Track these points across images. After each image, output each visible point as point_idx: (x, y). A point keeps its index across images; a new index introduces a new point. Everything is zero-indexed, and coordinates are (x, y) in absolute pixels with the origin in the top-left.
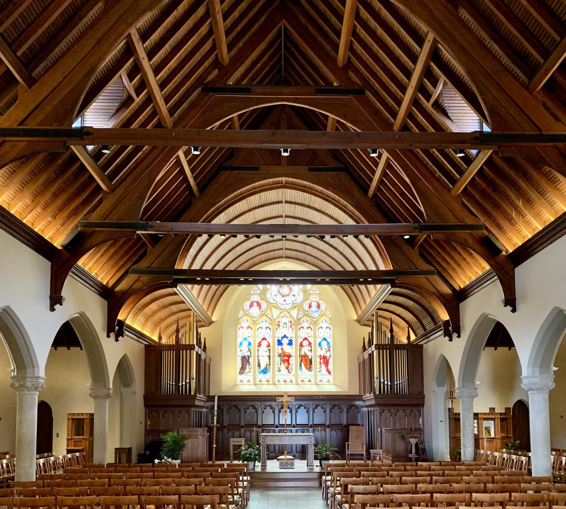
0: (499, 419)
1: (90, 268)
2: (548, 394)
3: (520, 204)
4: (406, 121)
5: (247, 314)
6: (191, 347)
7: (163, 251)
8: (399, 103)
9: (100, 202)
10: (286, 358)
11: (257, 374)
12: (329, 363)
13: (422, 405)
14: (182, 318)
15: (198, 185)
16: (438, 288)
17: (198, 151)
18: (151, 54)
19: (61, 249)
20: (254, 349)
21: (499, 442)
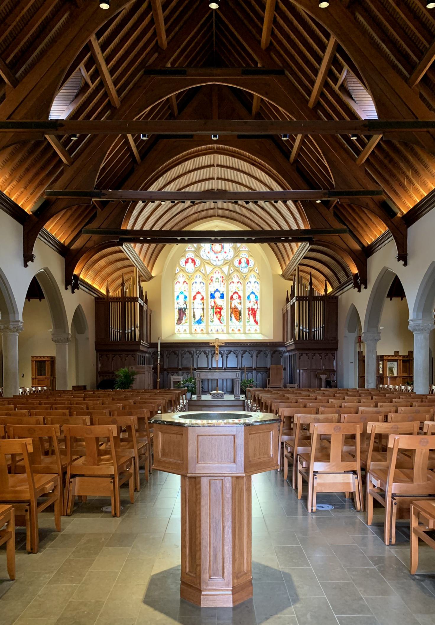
0: (401, 361)
1: (51, 230)
2: (429, 334)
3: (410, 174)
4: (319, 99)
5: (183, 270)
6: (135, 299)
7: (111, 213)
8: (313, 83)
9: (62, 173)
10: (218, 310)
11: (192, 324)
12: (257, 314)
13: (336, 349)
14: (126, 273)
15: (139, 152)
16: (348, 243)
17: (146, 137)
18: (103, 48)
19: (31, 215)
20: (190, 301)
21: (400, 380)
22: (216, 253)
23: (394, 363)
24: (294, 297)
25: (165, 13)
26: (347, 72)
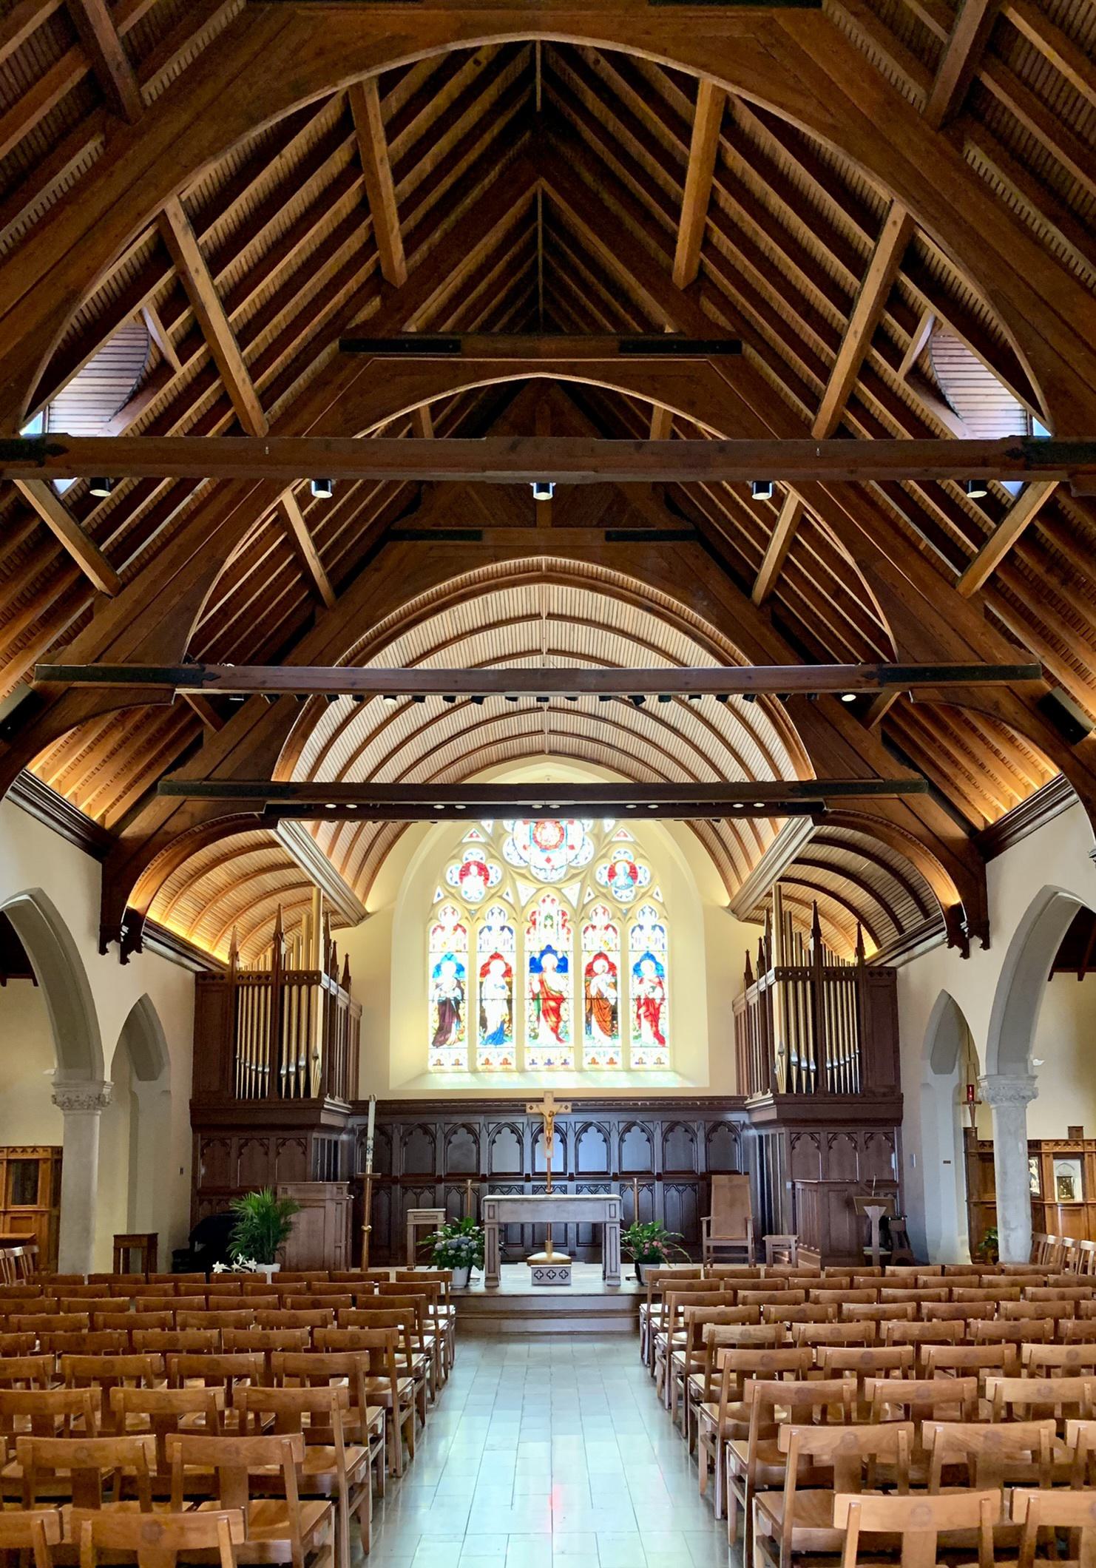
5: (452, 895)
9: (87, 617)
10: (551, 1005)
11: (478, 1045)
12: (661, 1015)
13: (898, 1121)
14: (290, 906)
15: (330, 575)
22: (545, 849)
23: (1070, 1162)
24: (770, 968)
25: (393, 145)
26: (934, 325)
